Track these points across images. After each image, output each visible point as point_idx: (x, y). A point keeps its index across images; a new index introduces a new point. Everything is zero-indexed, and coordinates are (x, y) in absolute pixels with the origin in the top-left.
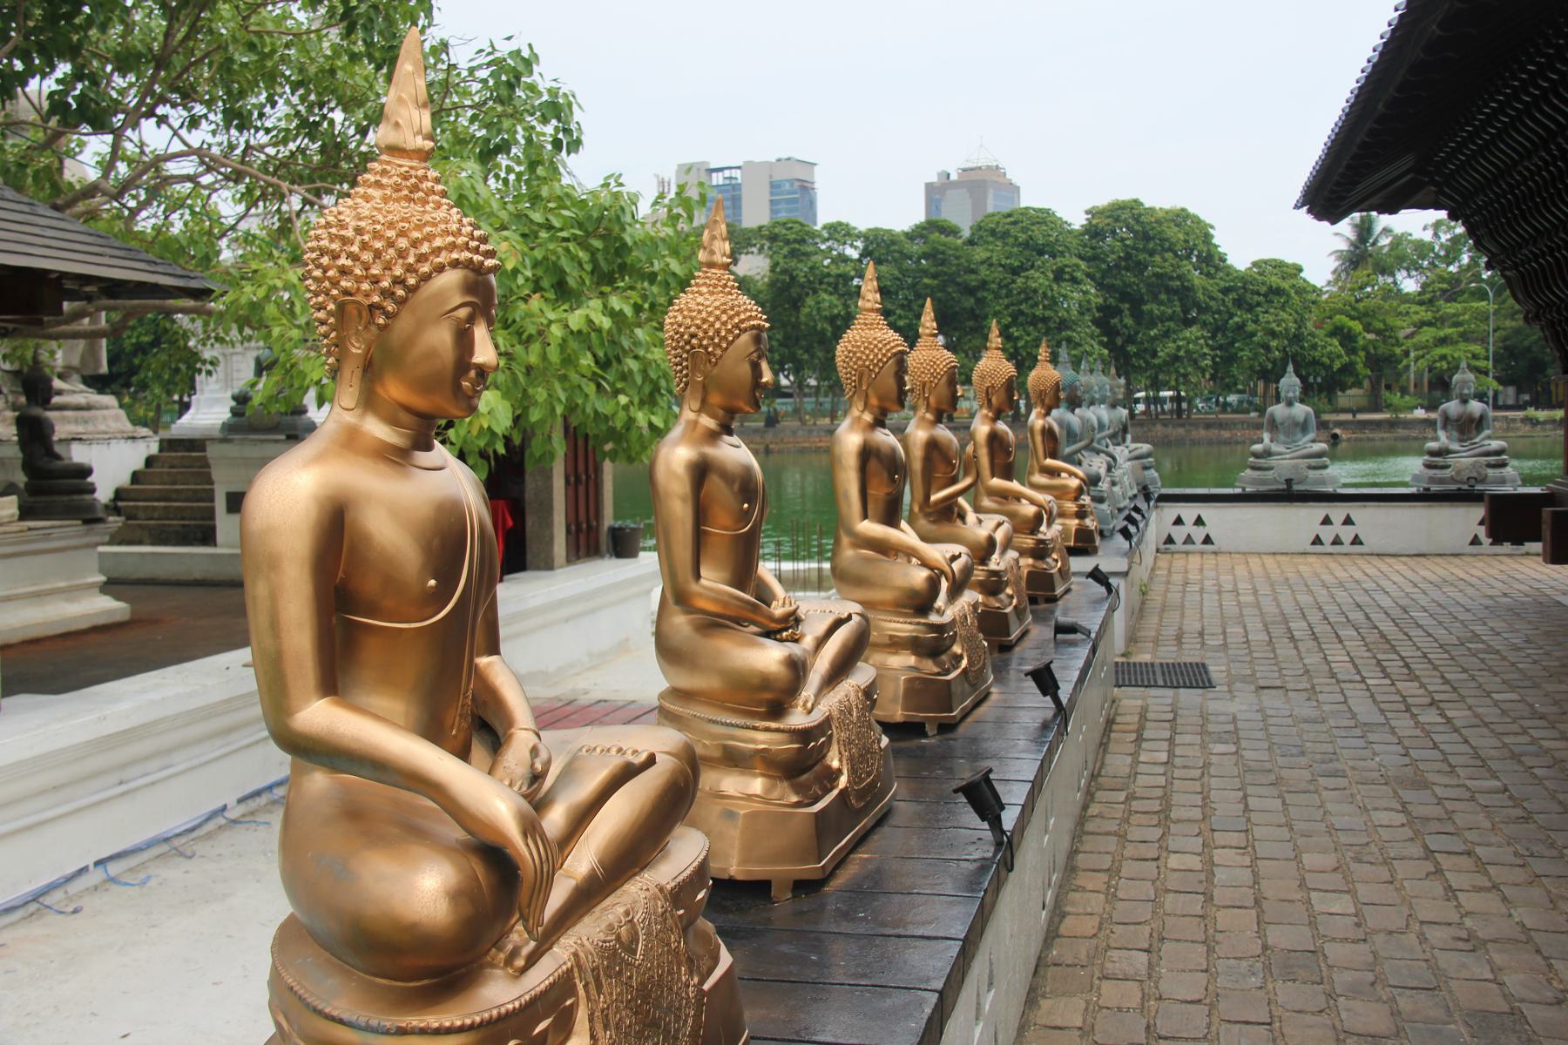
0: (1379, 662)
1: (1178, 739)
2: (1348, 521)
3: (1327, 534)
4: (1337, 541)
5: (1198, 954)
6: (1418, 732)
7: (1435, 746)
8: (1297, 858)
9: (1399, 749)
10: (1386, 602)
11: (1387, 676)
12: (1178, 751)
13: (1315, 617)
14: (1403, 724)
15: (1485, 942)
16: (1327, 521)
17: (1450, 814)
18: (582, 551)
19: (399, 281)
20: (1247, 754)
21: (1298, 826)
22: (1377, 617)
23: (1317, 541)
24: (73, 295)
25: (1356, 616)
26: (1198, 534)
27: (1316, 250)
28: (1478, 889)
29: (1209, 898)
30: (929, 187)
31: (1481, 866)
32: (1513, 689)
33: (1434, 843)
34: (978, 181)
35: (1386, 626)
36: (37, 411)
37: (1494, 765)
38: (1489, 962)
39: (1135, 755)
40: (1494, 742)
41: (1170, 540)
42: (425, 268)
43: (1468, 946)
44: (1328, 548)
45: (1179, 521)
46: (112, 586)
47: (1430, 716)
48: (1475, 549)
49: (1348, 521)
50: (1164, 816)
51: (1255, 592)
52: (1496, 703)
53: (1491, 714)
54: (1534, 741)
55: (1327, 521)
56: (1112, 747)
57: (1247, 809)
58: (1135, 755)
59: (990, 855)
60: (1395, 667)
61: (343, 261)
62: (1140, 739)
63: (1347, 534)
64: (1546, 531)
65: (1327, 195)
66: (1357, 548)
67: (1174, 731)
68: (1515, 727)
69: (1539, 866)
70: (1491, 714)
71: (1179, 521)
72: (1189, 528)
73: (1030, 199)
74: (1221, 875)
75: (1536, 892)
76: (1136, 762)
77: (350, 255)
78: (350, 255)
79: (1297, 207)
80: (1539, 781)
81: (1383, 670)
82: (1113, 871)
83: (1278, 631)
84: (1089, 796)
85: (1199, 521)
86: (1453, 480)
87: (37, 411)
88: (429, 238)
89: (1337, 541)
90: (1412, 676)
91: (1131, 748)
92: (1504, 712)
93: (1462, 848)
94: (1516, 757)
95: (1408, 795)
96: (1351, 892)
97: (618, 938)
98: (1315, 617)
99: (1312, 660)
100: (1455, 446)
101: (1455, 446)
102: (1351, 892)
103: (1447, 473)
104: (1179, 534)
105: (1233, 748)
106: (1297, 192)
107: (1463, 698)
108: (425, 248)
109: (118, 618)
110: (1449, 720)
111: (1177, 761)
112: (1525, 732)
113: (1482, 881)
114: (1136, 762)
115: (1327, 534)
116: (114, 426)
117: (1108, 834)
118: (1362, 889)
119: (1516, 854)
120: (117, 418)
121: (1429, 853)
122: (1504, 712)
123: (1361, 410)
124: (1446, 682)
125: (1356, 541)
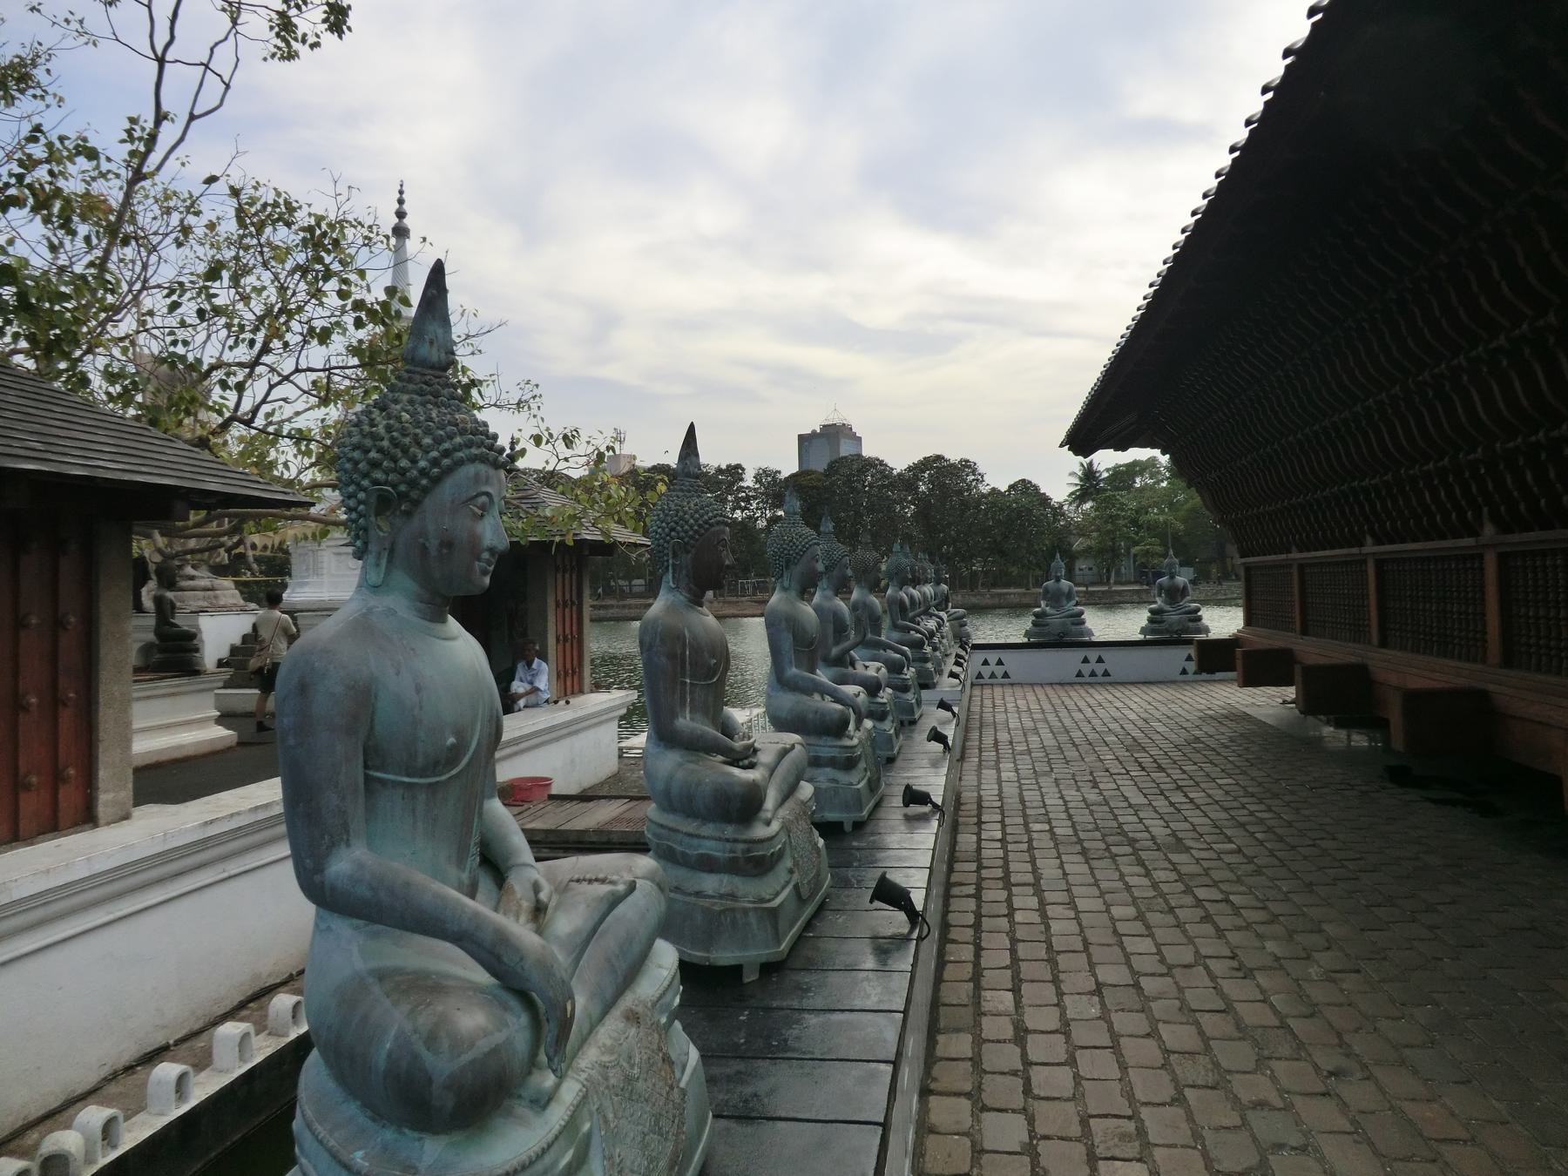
0: (1136, 760)
1: (1007, 821)
2: (1100, 660)
3: (1086, 669)
4: (1093, 674)
5: (1049, 992)
6: (1172, 810)
7: (1186, 820)
8: (1108, 911)
9: (1162, 823)
10: (1133, 716)
11: (1143, 769)
12: (1009, 830)
13: (1087, 729)
14: (1160, 803)
15: (1251, 970)
16: (1086, 660)
17: (1207, 872)
18: (30, 804)
19: (423, 473)
20: (1057, 831)
21: (1104, 885)
22: (1129, 727)
23: (1079, 674)
24: (197, 507)
25: (1114, 726)
26: (999, 671)
27: (1058, 477)
28: (1238, 929)
29: (1050, 947)
30: (801, 438)
31: (1237, 911)
32: (1230, 776)
33: (1202, 893)
34: (834, 433)
35: (1136, 733)
36: (170, 595)
37: (1229, 832)
38: (1258, 986)
39: (979, 834)
40: (1224, 815)
41: (980, 676)
42: (446, 462)
43: (1241, 974)
44: (1087, 679)
45: (986, 663)
46: (225, 718)
47: (1177, 798)
48: (1183, 677)
49: (1100, 660)
50: (1007, 882)
51: (1043, 712)
52: (1220, 786)
53: (1218, 794)
54: (1252, 813)
55: (1086, 660)
56: (961, 828)
57: (1065, 874)
58: (979, 834)
59: (906, 931)
60: (1147, 761)
61: (373, 454)
62: (980, 823)
63: (1099, 669)
64: (1239, 664)
65: (1082, 439)
66: (1107, 679)
67: (1003, 814)
68: (1235, 804)
69: (1276, 908)
70: (1218, 794)
71: (986, 663)
72: (993, 667)
73: (868, 451)
74: (1055, 927)
75: (1277, 929)
76: (979, 840)
77: (380, 450)
78: (380, 450)
79: (1061, 446)
80: (1261, 843)
81: (1140, 764)
82: (977, 927)
83: (1063, 738)
84: (951, 870)
85: (1000, 663)
86: (1167, 631)
87: (170, 595)
88: (450, 437)
89: (1093, 674)
90: (1161, 769)
91: (975, 829)
92: (1227, 793)
93: (1220, 897)
94: (1242, 825)
95: (1175, 857)
96: (1151, 935)
97: (529, 664)
98: (1087, 729)
99: (1090, 758)
100: (1168, 608)
101: (1168, 608)
102: (1151, 935)
103: (1163, 626)
104: (986, 671)
105: (1047, 827)
106: (1062, 436)
107: (1197, 784)
108: (446, 445)
109: (228, 743)
110: (1192, 801)
111: (1009, 838)
112: (1244, 807)
113: (1239, 922)
114: (979, 840)
115: (1086, 669)
116: (232, 601)
117: (968, 896)
118: (1158, 932)
119: (1257, 898)
120: (233, 596)
121: (1199, 903)
122: (1227, 793)
123: (1093, 584)
124: (1184, 772)
125: (1106, 674)
